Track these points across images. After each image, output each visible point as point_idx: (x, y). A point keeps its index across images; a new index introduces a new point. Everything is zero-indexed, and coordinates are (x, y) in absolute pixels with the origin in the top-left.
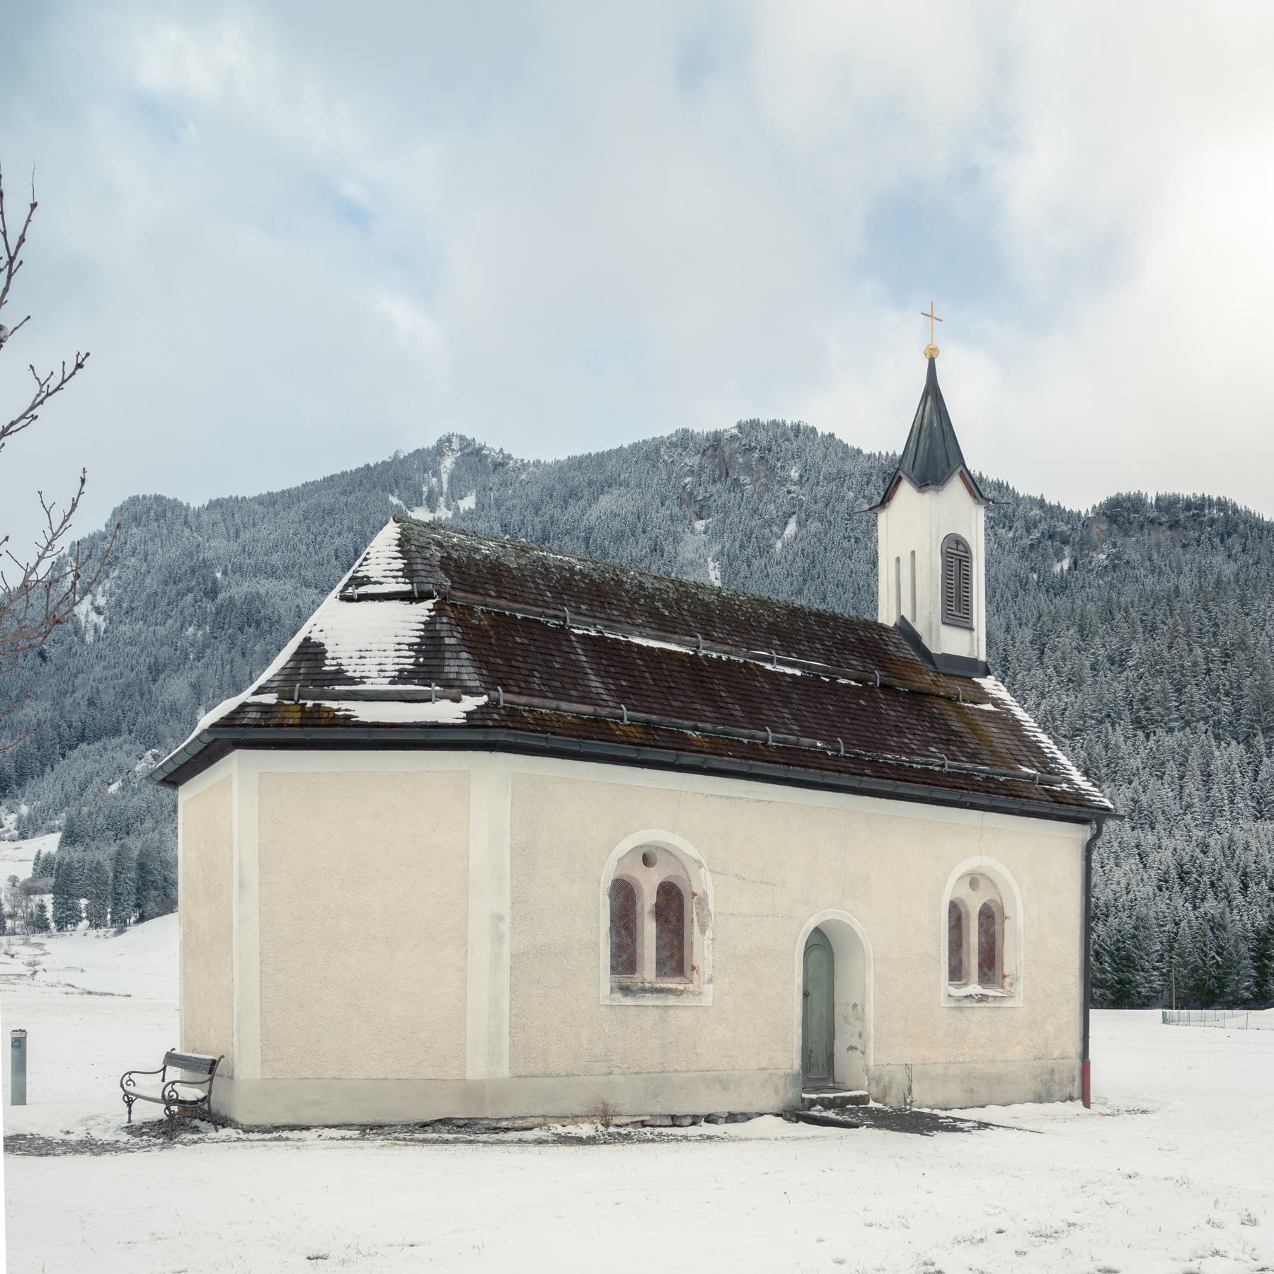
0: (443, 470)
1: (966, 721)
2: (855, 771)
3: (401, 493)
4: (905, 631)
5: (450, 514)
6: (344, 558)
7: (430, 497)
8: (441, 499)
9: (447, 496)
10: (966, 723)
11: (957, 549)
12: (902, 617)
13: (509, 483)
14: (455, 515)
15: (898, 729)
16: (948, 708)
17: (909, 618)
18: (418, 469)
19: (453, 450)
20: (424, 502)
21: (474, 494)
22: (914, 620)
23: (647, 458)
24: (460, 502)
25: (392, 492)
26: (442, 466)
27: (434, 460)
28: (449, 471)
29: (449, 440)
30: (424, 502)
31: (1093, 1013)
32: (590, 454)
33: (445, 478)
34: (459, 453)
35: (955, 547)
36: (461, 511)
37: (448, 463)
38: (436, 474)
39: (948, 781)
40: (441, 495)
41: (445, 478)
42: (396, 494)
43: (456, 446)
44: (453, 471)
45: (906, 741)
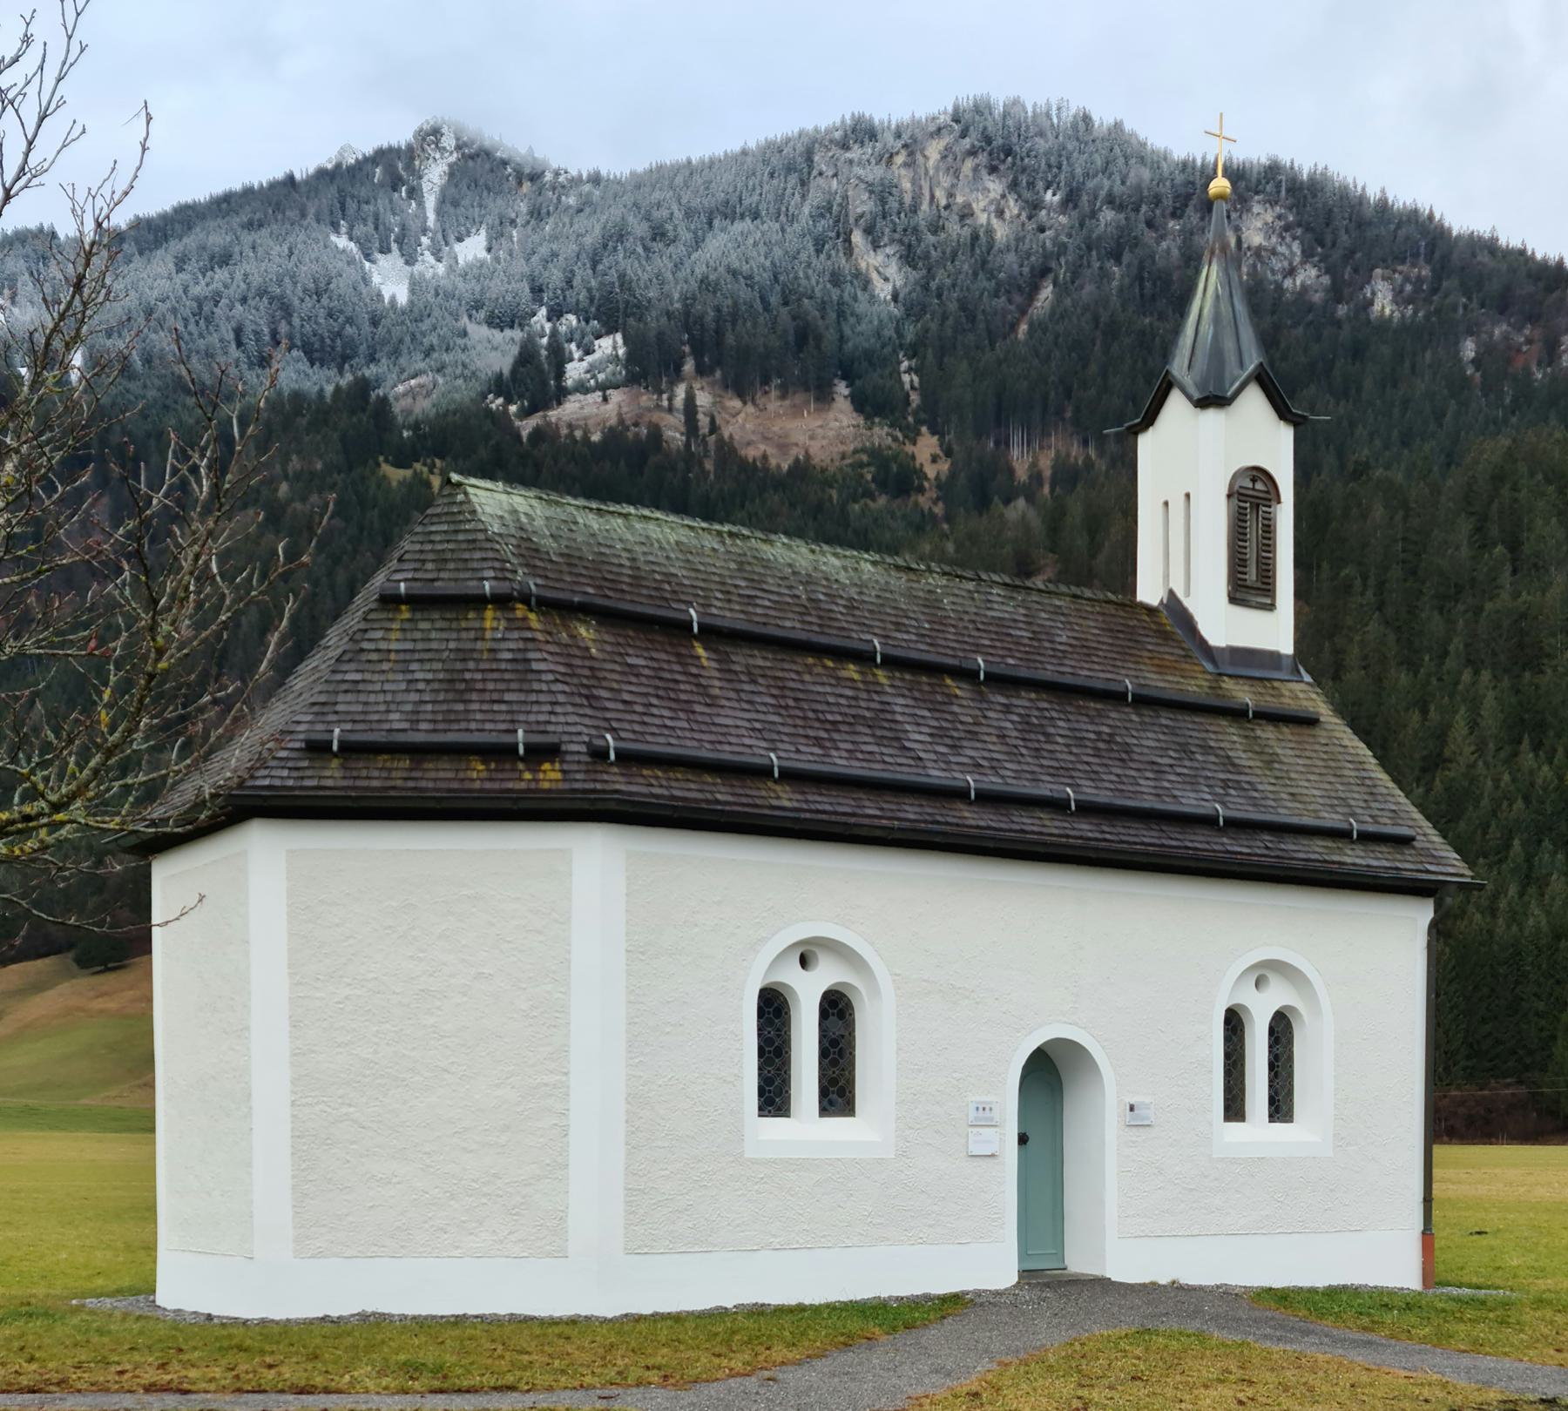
0: (426, 186)
1: (1257, 749)
2: (1090, 835)
3: (351, 228)
4: (1176, 610)
5: (441, 269)
6: (251, 345)
7: (404, 236)
8: (425, 240)
9: (435, 233)
10: (1257, 753)
11: (1254, 489)
12: (1171, 593)
13: (544, 211)
14: (451, 269)
15: (1156, 768)
16: (1232, 730)
17: (1180, 594)
18: (381, 184)
19: (444, 148)
20: (394, 246)
21: (483, 232)
22: (1188, 594)
23: (790, 169)
24: (458, 247)
25: (335, 227)
26: (425, 179)
27: (409, 167)
28: (436, 189)
29: (436, 132)
30: (394, 246)
31: (1438, 1150)
32: (689, 162)
33: (430, 202)
34: (455, 155)
35: (1251, 485)
36: (461, 261)
37: (434, 175)
38: (414, 193)
39: (1223, 844)
40: (424, 231)
41: (430, 202)
42: (343, 230)
43: (448, 142)
44: (443, 190)
45: (1166, 784)
